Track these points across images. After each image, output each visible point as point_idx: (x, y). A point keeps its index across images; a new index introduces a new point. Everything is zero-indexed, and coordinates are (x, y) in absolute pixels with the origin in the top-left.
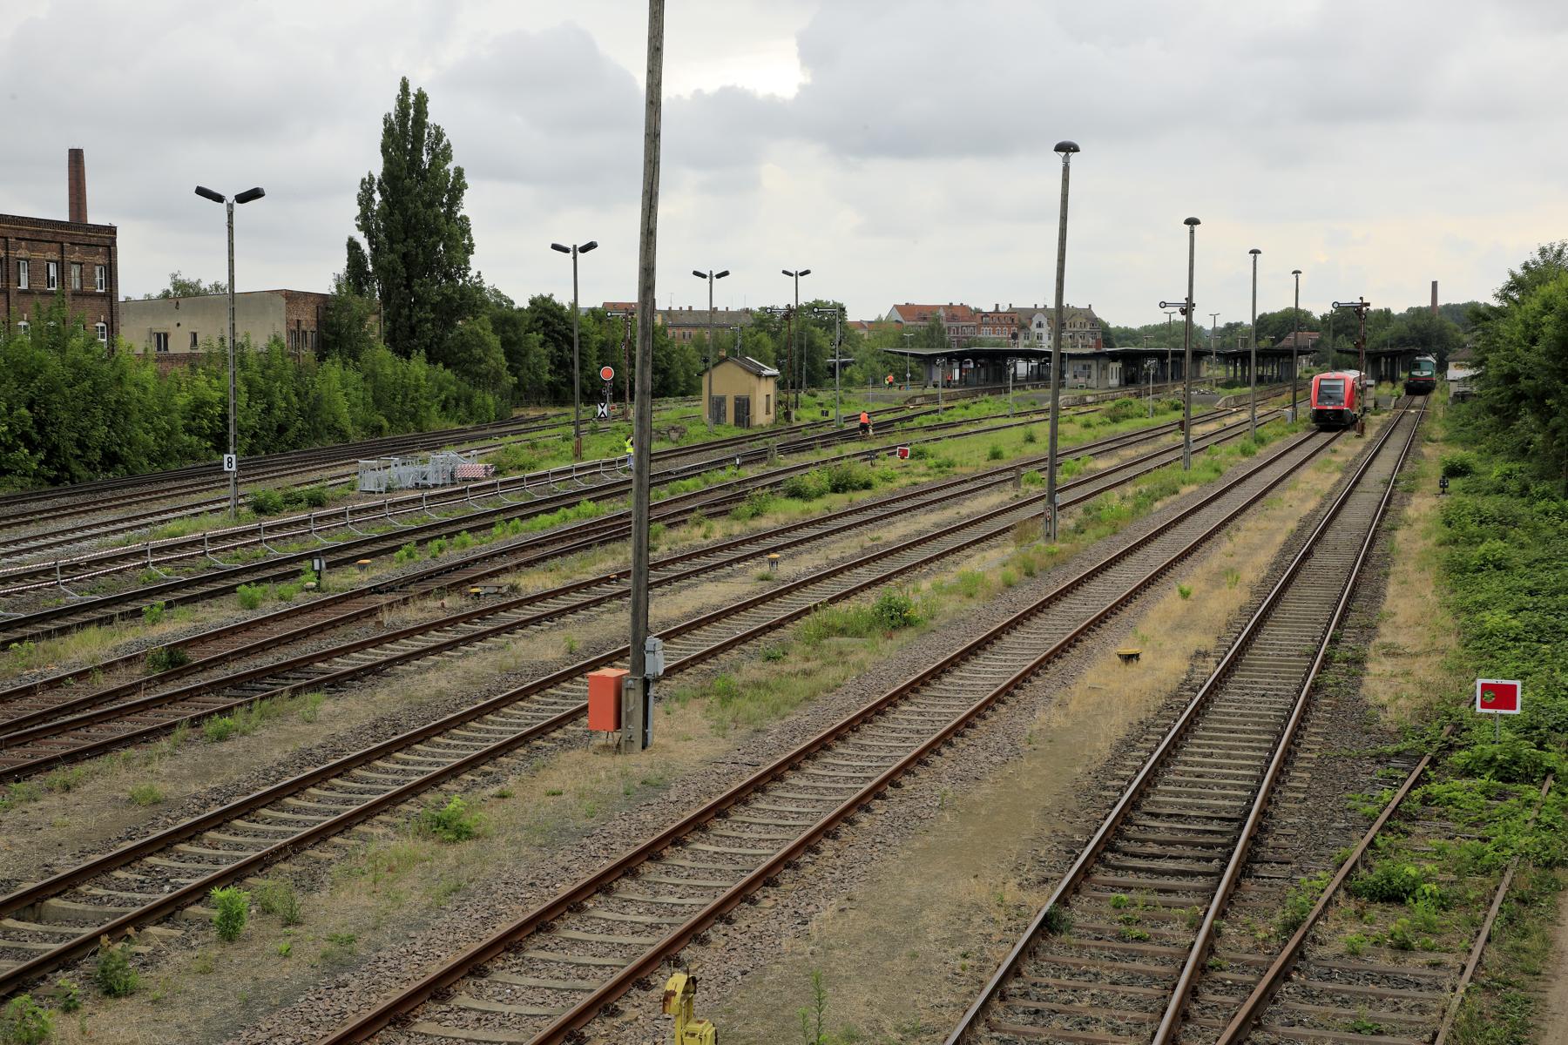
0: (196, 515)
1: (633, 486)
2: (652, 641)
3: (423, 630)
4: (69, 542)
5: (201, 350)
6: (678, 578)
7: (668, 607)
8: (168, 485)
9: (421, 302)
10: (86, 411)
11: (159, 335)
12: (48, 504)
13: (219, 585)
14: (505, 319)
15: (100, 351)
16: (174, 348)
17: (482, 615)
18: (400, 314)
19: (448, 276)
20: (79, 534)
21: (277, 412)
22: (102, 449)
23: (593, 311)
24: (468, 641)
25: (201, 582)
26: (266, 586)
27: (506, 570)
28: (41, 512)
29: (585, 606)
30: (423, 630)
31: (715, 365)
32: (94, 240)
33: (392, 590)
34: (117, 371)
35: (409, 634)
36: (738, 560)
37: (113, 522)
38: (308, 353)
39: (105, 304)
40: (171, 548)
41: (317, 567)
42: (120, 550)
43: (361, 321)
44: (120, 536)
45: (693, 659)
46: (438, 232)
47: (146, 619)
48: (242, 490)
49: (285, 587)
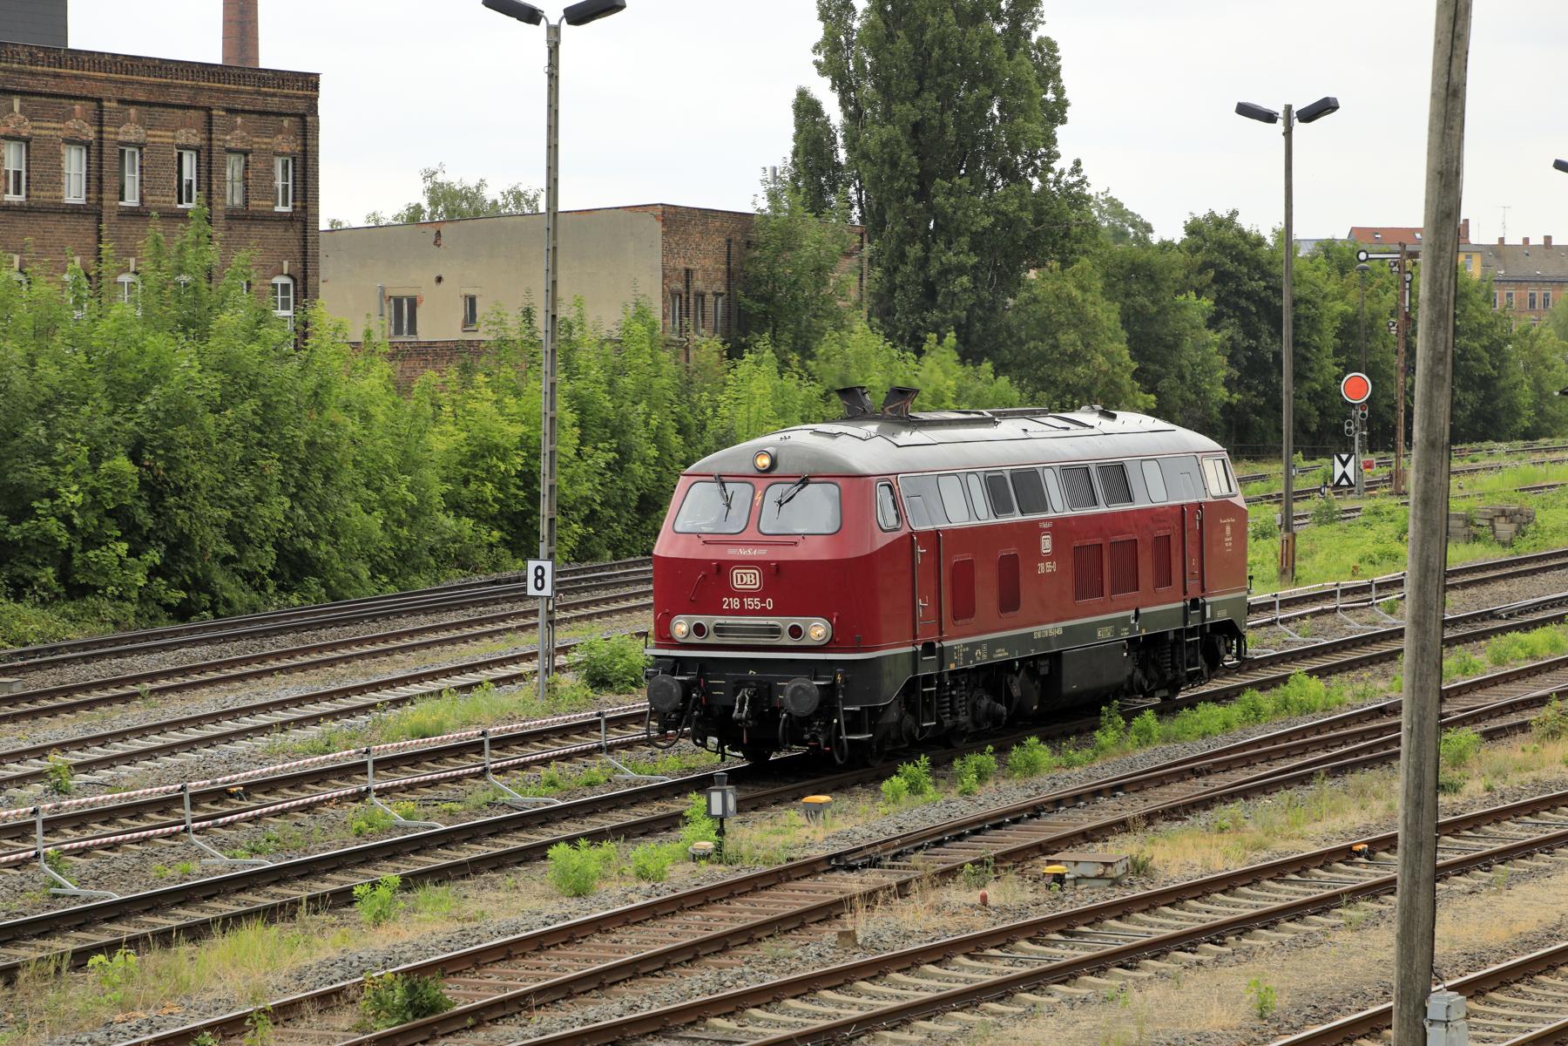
0: (467, 688)
2: (1440, 1001)
3: (940, 954)
5: (483, 334)
6: (1505, 856)
8: (409, 624)
9: (948, 230)
10: (247, 463)
11: (398, 302)
12: (169, 660)
13: (513, 843)
14: (1138, 272)
15: (277, 336)
16: (427, 331)
17: (1066, 925)
18: (903, 257)
20: (228, 726)
21: (638, 468)
22: (278, 545)
23: (1327, 248)
24: (1036, 981)
25: (473, 834)
26: (608, 847)
27: (1123, 826)
28: (152, 677)
29: (1295, 912)
30: (940, 954)
32: (273, 104)
33: (874, 863)
34: (312, 381)
35: (909, 962)
37: (298, 702)
38: (708, 345)
39: (292, 235)
40: (414, 760)
41: (717, 809)
43: (820, 271)
44: (312, 731)
47: (362, 912)
48: (563, 636)
49: (645, 851)
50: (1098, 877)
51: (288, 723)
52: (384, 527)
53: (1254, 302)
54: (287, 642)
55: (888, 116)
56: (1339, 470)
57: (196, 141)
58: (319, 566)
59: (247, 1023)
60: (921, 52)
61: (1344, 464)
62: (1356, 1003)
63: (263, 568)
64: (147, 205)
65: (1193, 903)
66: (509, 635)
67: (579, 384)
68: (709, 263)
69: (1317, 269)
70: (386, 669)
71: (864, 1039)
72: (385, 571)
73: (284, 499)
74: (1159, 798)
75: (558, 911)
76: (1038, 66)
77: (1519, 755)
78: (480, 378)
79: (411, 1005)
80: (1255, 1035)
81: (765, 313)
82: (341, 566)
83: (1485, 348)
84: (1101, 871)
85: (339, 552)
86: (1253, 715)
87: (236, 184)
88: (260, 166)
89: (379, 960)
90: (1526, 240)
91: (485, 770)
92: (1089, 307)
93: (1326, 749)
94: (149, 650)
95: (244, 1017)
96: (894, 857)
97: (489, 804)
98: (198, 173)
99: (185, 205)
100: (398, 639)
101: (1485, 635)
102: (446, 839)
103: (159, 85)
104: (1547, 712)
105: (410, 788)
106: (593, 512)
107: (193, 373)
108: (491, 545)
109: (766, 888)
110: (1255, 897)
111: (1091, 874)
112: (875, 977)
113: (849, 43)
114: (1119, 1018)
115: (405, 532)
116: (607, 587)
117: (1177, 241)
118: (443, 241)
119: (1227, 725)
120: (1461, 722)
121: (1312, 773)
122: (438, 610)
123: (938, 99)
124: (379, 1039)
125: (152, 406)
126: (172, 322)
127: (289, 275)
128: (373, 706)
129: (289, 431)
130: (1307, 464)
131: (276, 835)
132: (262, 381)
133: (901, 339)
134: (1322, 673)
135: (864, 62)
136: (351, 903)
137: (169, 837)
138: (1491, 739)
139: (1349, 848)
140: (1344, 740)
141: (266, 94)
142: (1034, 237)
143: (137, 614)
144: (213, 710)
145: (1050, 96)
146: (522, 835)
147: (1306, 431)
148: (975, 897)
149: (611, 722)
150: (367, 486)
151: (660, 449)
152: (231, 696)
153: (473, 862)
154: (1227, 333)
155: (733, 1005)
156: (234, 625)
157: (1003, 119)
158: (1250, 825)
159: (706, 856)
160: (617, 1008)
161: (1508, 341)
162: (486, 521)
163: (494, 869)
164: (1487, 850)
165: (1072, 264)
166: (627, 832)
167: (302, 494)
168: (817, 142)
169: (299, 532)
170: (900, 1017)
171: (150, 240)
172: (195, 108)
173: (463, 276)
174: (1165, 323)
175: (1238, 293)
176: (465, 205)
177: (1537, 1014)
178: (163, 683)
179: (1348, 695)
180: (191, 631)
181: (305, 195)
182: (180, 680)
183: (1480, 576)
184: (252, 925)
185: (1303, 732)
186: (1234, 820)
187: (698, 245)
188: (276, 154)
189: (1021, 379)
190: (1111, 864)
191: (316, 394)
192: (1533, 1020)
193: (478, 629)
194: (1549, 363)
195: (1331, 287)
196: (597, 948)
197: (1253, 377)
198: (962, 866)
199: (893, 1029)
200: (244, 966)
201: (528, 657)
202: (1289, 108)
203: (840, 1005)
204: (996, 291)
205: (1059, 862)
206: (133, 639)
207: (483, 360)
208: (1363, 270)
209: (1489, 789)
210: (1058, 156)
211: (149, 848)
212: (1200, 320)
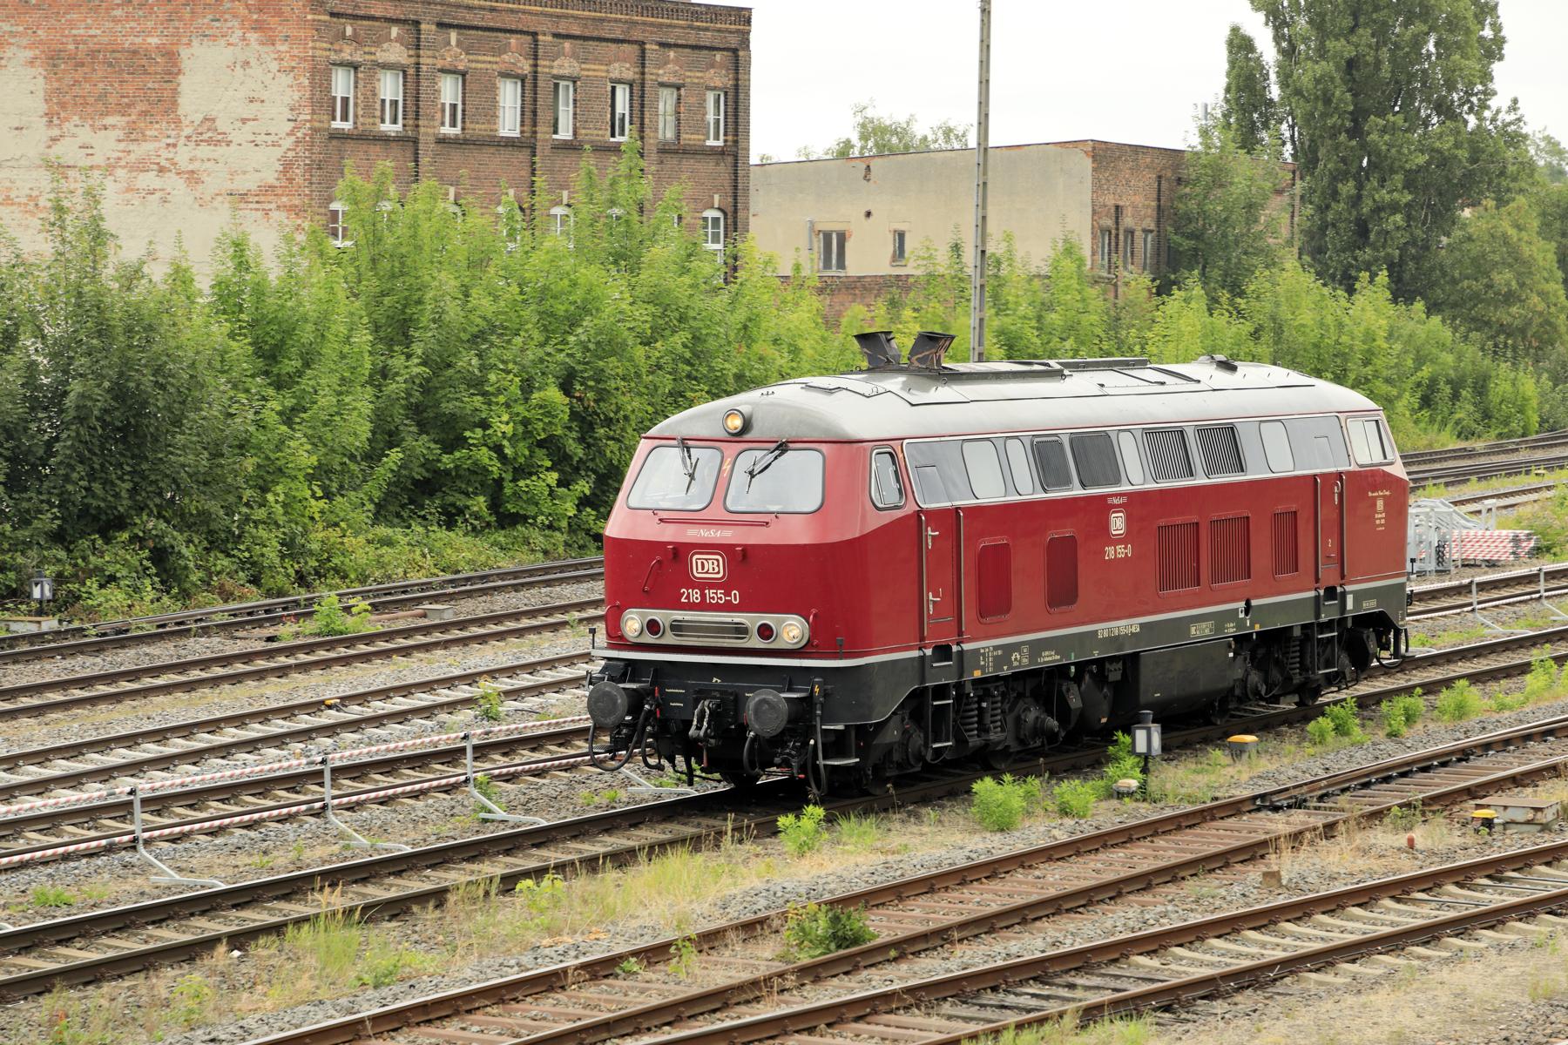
3: (1366, 896)
5: (912, 268)
9: (1382, 168)
11: (827, 236)
15: (707, 269)
17: (1495, 870)
18: (1335, 194)
24: (1462, 926)
30: (1366, 896)
32: (706, 38)
33: (1299, 804)
34: (741, 315)
35: (1334, 903)
38: (1137, 281)
43: (1251, 208)
50: (1528, 822)
55: (1322, 53)
59: (672, 950)
67: (1006, 319)
71: (1288, 980)
79: (834, 936)
81: (1196, 250)
84: (1530, 816)
88: (692, 100)
89: (803, 891)
95: (667, 945)
96: (1321, 798)
99: (618, 139)
103: (594, 19)
109: (1190, 827)
111: (1521, 819)
112: (1299, 919)
123: (1373, 36)
125: (583, 338)
126: (603, 255)
129: (718, 363)
132: (692, 313)
133: (1333, 277)
141: (699, 28)
142: (1469, 175)
143: (566, 544)
145: (1488, 33)
148: (1401, 840)
157: (1439, 56)
165: (1507, 202)
171: (583, 173)
172: (629, 42)
173: (893, 211)
176: (894, 140)
181: (736, 130)
187: (1128, 181)
188: (709, 88)
189: (1454, 318)
191: (745, 327)
196: (1020, 883)
198: (1389, 809)
199: (1318, 970)
203: (1264, 945)
205: (1488, 806)
206: (562, 569)
207: (912, 295)
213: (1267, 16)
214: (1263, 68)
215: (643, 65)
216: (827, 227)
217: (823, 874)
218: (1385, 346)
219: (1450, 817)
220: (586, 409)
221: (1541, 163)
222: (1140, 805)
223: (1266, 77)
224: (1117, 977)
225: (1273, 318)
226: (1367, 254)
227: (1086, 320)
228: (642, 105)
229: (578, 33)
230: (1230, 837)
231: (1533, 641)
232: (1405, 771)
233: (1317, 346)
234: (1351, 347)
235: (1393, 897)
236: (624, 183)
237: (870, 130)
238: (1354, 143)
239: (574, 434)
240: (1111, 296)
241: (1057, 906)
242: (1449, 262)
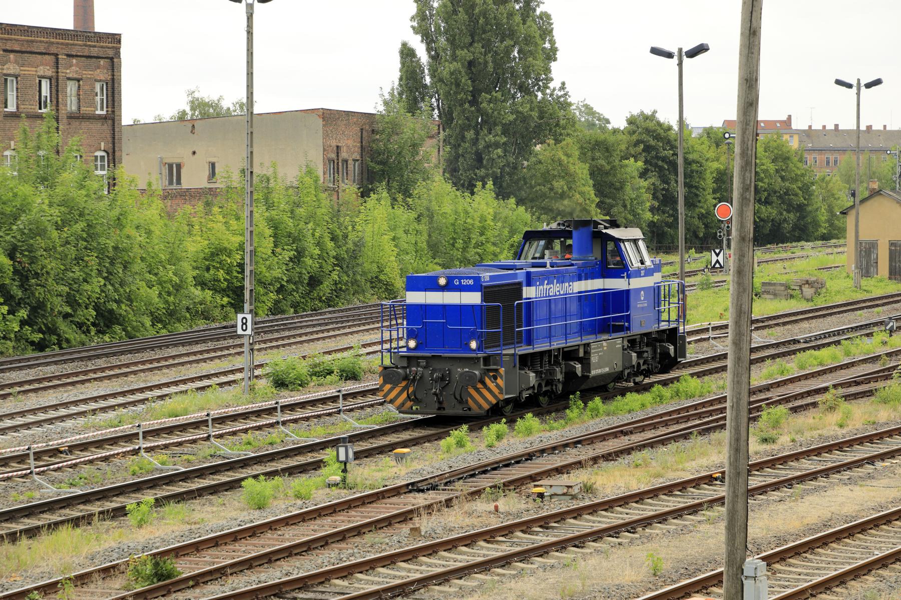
0: (202, 389)
1: (729, 362)
2: (752, 563)
3: (470, 540)
4: (50, 421)
5: (220, 184)
6: (801, 479)
7: (777, 519)
8: (173, 351)
9: (489, 123)
10: (78, 259)
11: (170, 166)
12: (31, 374)
13: (224, 478)
14: (599, 147)
15: (95, 185)
16: (187, 182)
17: (544, 522)
18: (463, 138)
19: (523, 88)
20: (63, 412)
21: (308, 261)
22: (97, 308)
23: (709, 132)
24: (524, 555)
25: (201, 473)
26: (278, 479)
27: (579, 464)
28: (20, 384)
29: (677, 513)
30: (470, 540)
31: (863, 201)
32: (94, 52)
33: (434, 488)
34: (116, 212)
35: (451, 545)
36: (882, 457)
37: (104, 397)
38: (350, 189)
39: (106, 128)
40: (170, 430)
41: (342, 457)
42: (109, 433)
43: (415, 146)
44: (111, 415)
45: (814, 587)
46: (512, 34)
47: (131, 520)
48: (259, 358)
49: (300, 482)
50: (564, 494)
51: (96, 410)
52: (160, 295)
53: (666, 163)
54: (101, 363)
55: (454, 58)
56: (714, 258)
57: (49, 73)
58: (121, 319)
59: (59, 586)
60: (473, 19)
61: (717, 255)
62: (710, 566)
63: (88, 320)
64: (21, 110)
65: (619, 509)
66: (230, 358)
67: (273, 212)
68: (350, 143)
69: (703, 143)
70: (157, 378)
71: (422, 591)
72: (161, 321)
73: (101, 279)
74: (602, 448)
75: (247, 518)
76: (540, 28)
77: (811, 421)
78: (216, 209)
79: (156, 574)
80: (650, 586)
81: (383, 171)
82: (134, 319)
83: (800, 188)
84: (565, 491)
85: (133, 310)
86: (658, 400)
87: (73, 98)
88: (87, 88)
89: (140, 548)
90: (824, 127)
91: (209, 436)
92: (571, 166)
93: (700, 418)
94: (20, 368)
95: (57, 583)
96: (446, 484)
97: (211, 456)
98: (51, 91)
99: (43, 110)
100: (151, 363)
101: (794, 352)
102: (185, 476)
103: (27, 41)
104: (828, 396)
105: (166, 447)
106: (282, 286)
107: (45, 207)
108: (223, 306)
109: (370, 503)
110: (655, 505)
111: (560, 492)
112: (430, 554)
113: (431, 15)
114: (571, 577)
115: (171, 299)
116: (289, 329)
117: (622, 128)
118: (196, 130)
119: (643, 405)
120: (779, 402)
121: (691, 433)
122: (190, 343)
123: (483, 47)
124: (137, 595)
125: (21, 227)
126: (34, 178)
127: (104, 150)
128: (147, 399)
129: (102, 240)
130: (698, 255)
131: (85, 475)
132: (87, 212)
133: (463, 185)
134: (699, 375)
135: (440, 26)
136: (126, 515)
137: (22, 477)
138: (796, 412)
139: (711, 476)
140: (710, 413)
141: (90, 46)
142: (539, 126)
143: (14, 347)
144: (55, 403)
145: (547, 45)
146: (230, 473)
147: (697, 237)
148: (491, 507)
149: (284, 408)
150: (150, 272)
151: (321, 250)
152: (65, 395)
153: (198, 490)
154: (652, 180)
155: (346, 572)
156: (71, 354)
157: (520, 59)
158: (654, 463)
159: (336, 485)
160: (278, 574)
161: (813, 184)
162: (219, 292)
163: (211, 494)
164: (790, 476)
165: (561, 141)
166: (291, 471)
167: (111, 277)
168: (413, 72)
169: (108, 299)
170: (443, 578)
171: (21, 130)
172: (49, 54)
173: (208, 150)
174: (615, 176)
175: (657, 157)
176: (211, 110)
177: (816, 571)
178: (27, 387)
179: (714, 387)
180: (45, 357)
181: (113, 105)
182: (37, 386)
183: (794, 318)
184: (65, 528)
185: (687, 409)
186: (644, 460)
187: (344, 132)
188: (96, 81)
189: (532, 208)
190: (571, 487)
191: (119, 219)
192: (813, 575)
193: (213, 354)
194: (836, 196)
195: (711, 154)
196: (269, 539)
197: (666, 206)
198: (484, 489)
199: (440, 584)
200: (59, 552)
201: (240, 370)
202: (680, 50)
203: (409, 571)
204: (517, 158)
205: (541, 486)
206: (11, 362)
207: (218, 198)
208: (729, 144)
209: (793, 441)
210: (552, 80)
211: (10, 484)
212: (636, 174)
213: (422, 37)
214: (421, 66)
215: (57, 68)
216: (170, 161)
217: (152, 537)
218: (492, 224)
219: (520, 493)
220: (23, 268)
221: (583, 119)
222: (342, 491)
223: (423, 72)
224: (323, 592)
225: (428, 209)
226: (482, 172)
227: (319, 212)
228: (57, 91)
229: (18, 49)
230: (393, 508)
231: (323, 446)
232: (495, 467)
233: (453, 225)
234: (473, 225)
235: (485, 540)
236: (45, 136)
237: (197, 104)
238: (473, 108)
239: (17, 283)
240: (335, 197)
241: (289, 552)
242: (528, 175)
